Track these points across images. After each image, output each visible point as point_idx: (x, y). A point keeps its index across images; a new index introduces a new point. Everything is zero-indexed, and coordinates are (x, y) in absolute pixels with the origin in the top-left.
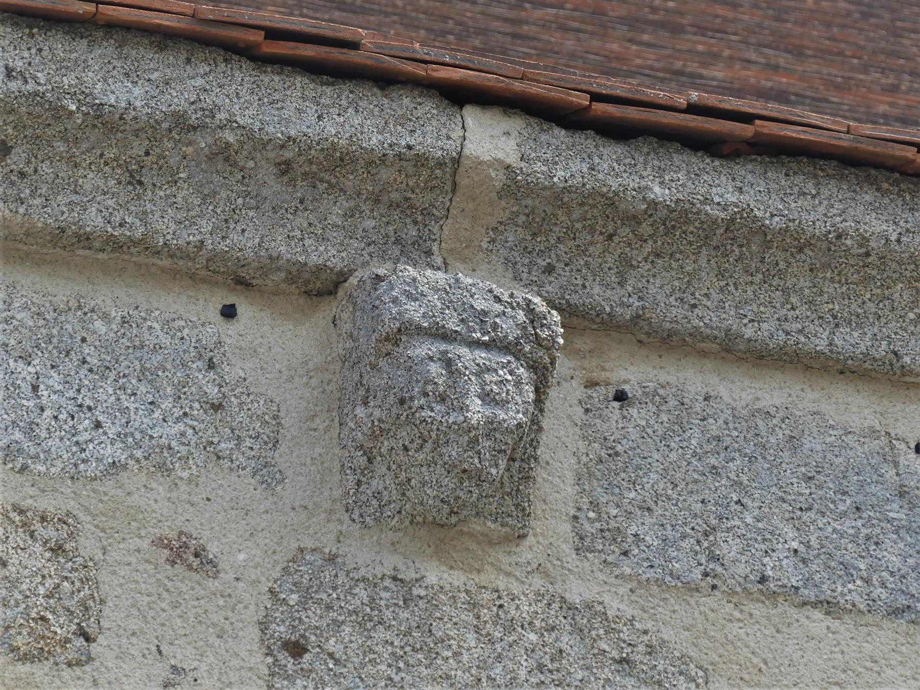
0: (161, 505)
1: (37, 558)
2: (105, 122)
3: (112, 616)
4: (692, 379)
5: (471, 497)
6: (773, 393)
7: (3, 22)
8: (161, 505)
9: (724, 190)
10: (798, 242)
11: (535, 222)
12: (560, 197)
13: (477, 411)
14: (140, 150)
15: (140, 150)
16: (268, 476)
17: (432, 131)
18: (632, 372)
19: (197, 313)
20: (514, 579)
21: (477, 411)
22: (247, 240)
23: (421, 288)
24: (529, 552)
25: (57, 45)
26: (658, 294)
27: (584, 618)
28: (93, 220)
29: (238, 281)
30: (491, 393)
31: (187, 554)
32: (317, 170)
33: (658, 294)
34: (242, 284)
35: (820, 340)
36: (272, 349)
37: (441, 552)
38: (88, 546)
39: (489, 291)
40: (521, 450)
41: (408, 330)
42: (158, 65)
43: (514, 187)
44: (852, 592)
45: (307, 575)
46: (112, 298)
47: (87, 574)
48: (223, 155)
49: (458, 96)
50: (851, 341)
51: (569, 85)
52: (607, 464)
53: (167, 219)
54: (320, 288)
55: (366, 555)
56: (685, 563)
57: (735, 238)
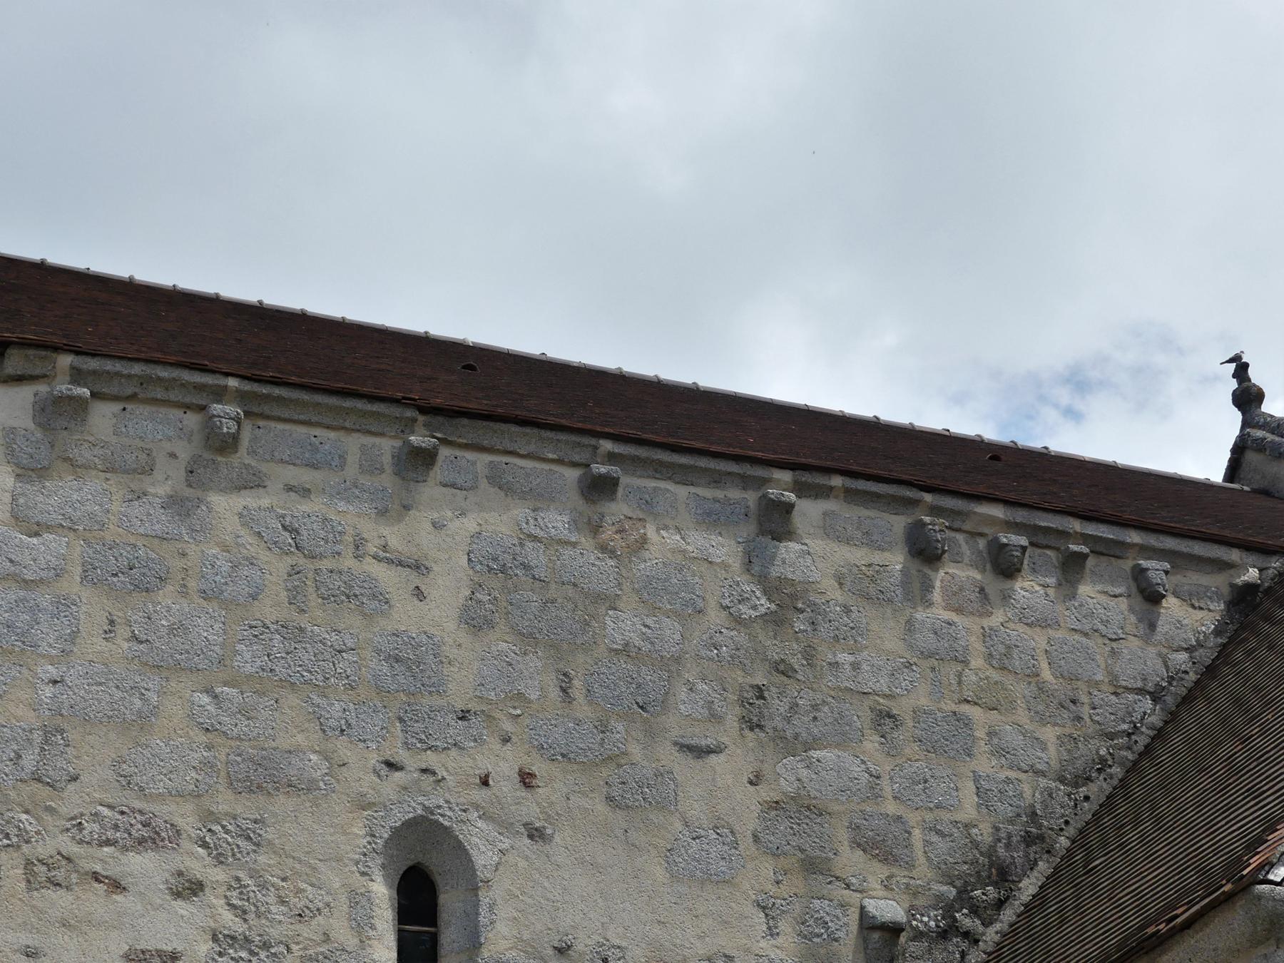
0: (168, 446)
1: (145, 456)
2: (160, 379)
3: (158, 466)
4: (273, 424)
5: (228, 445)
6: (288, 427)
7: (1281, 419)
8: (168, 446)
9: (277, 391)
10: (291, 400)
11: (242, 397)
12: (246, 392)
13: (225, 430)
14: (168, 384)
15: (168, 384)
16: (190, 441)
17: (222, 381)
18: (261, 423)
19: (178, 413)
20: (235, 460)
21: (225, 430)
22: (188, 400)
23: (217, 408)
24: (238, 455)
25: (152, 366)
26: (266, 409)
27: (247, 466)
28: (159, 396)
29: (187, 407)
30: (228, 427)
31: (173, 455)
32: (200, 388)
33: (266, 409)
34: (188, 408)
35: (296, 417)
36: (192, 420)
37: (221, 455)
38: (154, 454)
39: (232, 409)
40: (235, 438)
41: (214, 416)
42: (170, 369)
43: (237, 390)
44: (298, 462)
45: (196, 459)
46: (163, 410)
47: (153, 460)
48: (183, 385)
49: (227, 375)
50: (302, 417)
51: (248, 373)
52: (254, 439)
53: (173, 396)
54: (202, 408)
55: (207, 455)
56: (267, 457)
57: (280, 400)
